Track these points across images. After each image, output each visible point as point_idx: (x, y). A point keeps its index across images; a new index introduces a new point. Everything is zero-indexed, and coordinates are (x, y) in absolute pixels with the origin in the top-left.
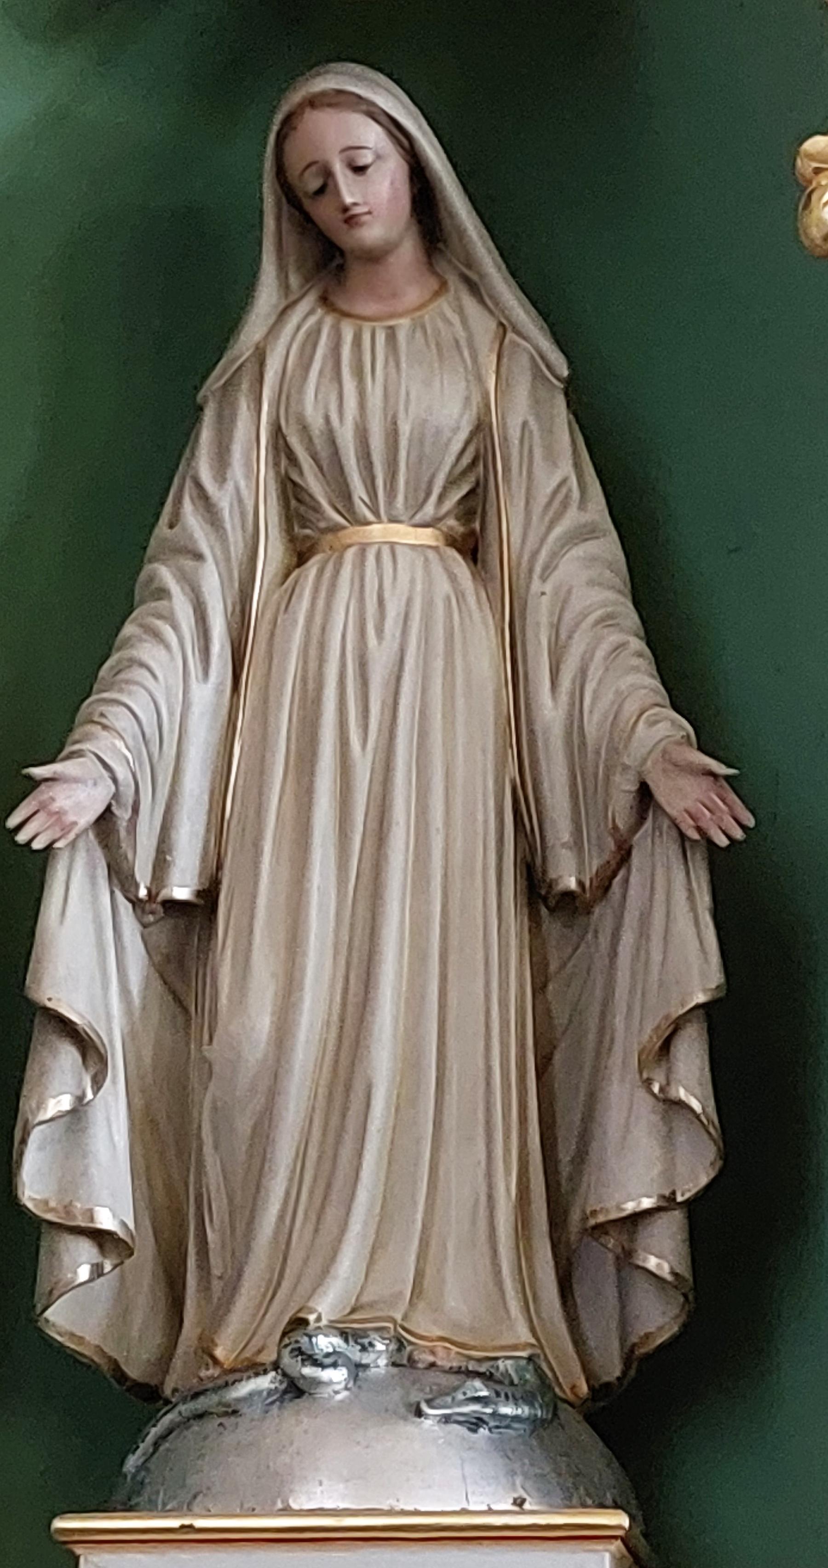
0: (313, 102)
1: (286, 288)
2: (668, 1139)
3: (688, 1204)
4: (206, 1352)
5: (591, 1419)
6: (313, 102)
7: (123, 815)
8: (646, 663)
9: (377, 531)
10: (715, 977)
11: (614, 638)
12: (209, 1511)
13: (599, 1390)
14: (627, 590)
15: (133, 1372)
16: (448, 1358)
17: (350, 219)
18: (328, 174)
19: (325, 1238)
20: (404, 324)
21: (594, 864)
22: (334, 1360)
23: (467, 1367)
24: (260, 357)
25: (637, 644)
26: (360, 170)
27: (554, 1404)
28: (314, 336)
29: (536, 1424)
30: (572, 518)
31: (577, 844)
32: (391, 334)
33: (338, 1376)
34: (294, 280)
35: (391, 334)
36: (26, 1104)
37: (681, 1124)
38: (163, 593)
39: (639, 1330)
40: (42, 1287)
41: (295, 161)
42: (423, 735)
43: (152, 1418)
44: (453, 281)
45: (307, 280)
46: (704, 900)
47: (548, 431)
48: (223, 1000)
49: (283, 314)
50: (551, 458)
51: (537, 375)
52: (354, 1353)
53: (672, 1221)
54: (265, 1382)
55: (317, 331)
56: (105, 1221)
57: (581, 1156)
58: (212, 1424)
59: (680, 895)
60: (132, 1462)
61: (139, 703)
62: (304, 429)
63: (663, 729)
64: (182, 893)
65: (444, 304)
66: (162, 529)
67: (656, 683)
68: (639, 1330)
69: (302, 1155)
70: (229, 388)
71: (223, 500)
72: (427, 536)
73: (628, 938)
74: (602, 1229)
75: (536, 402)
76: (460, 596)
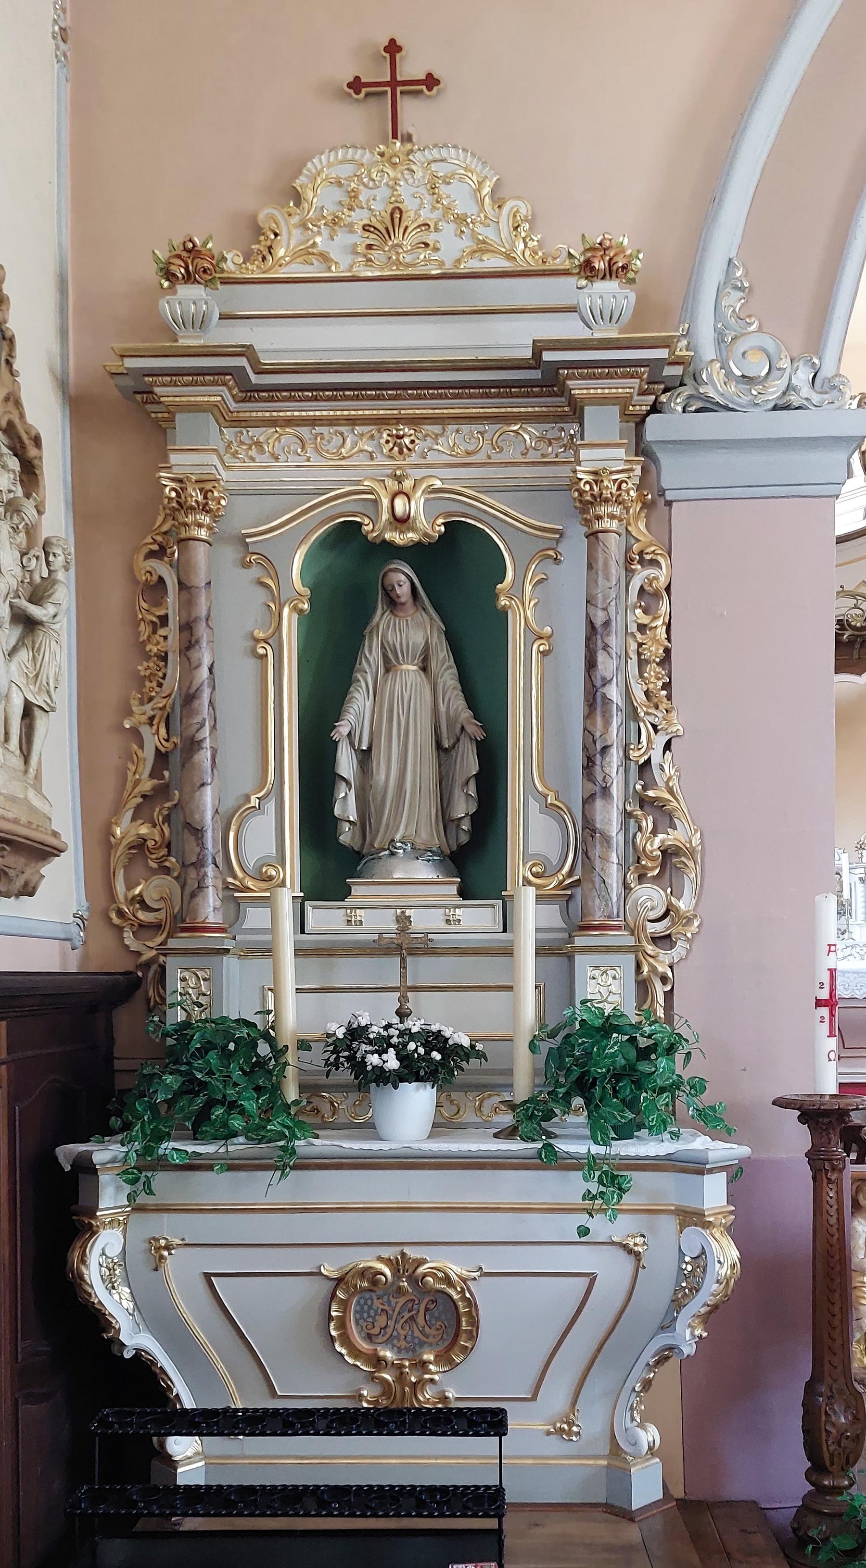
0: (391, 570)
1: (383, 608)
2: (467, 802)
3: (471, 815)
4: (372, 845)
5: (450, 859)
6: (391, 570)
7: (353, 732)
8: (463, 698)
9: (404, 667)
10: (477, 768)
11: (456, 692)
12: (202, 1005)
13: (452, 852)
14: (457, 678)
15: (356, 849)
16: (422, 847)
17: (398, 597)
18: (393, 587)
19: (397, 822)
20: (409, 618)
21: (452, 742)
22: (400, 848)
23: (606, 682)
24: (378, 626)
25: (461, 694)
26: (400, 586)
27: (445, 856)
28: (390, 620)
29: (441, 861)
30: (447, 664)
31: (448, 738)
32: (407, 621)
33: (401, 851)
34: (385, 608)
35: (407, 621)
36: (336, 794)
37: (470, 798)
38: (359, 681)
39: (460, 841)
40: (338, 831)
41: (386, 583)
42: (415, 714)
43: (361, 859)
44: (420, 608)
45: (388, 607)
46: (475, 751)
47: (441, 643)
48: (374, 771)
49: (382, 615)
50: (442, 650)
51: (438, 630)
52: (404, 846)
53: (468, 819)
54: (387, 852)
55: (390, 619)
56: (352, 819)
57: (448, 804)
58: (375, 861)
59: (470, 751)
60: (359, 868)
61: (356, 708)
62: (388, 642)
63: (467, 714)
64: (364, 748)
65: (418, 614)
66: (357, 665)
67: (464, 702)
68: (460, 841)
69: (391, 805)
70: (371, 632)
71: (371, 660)
72: (415, 668)
73: (459, 760)
74: (452, 821)
75: (439, 637)
76: (422, 680)
